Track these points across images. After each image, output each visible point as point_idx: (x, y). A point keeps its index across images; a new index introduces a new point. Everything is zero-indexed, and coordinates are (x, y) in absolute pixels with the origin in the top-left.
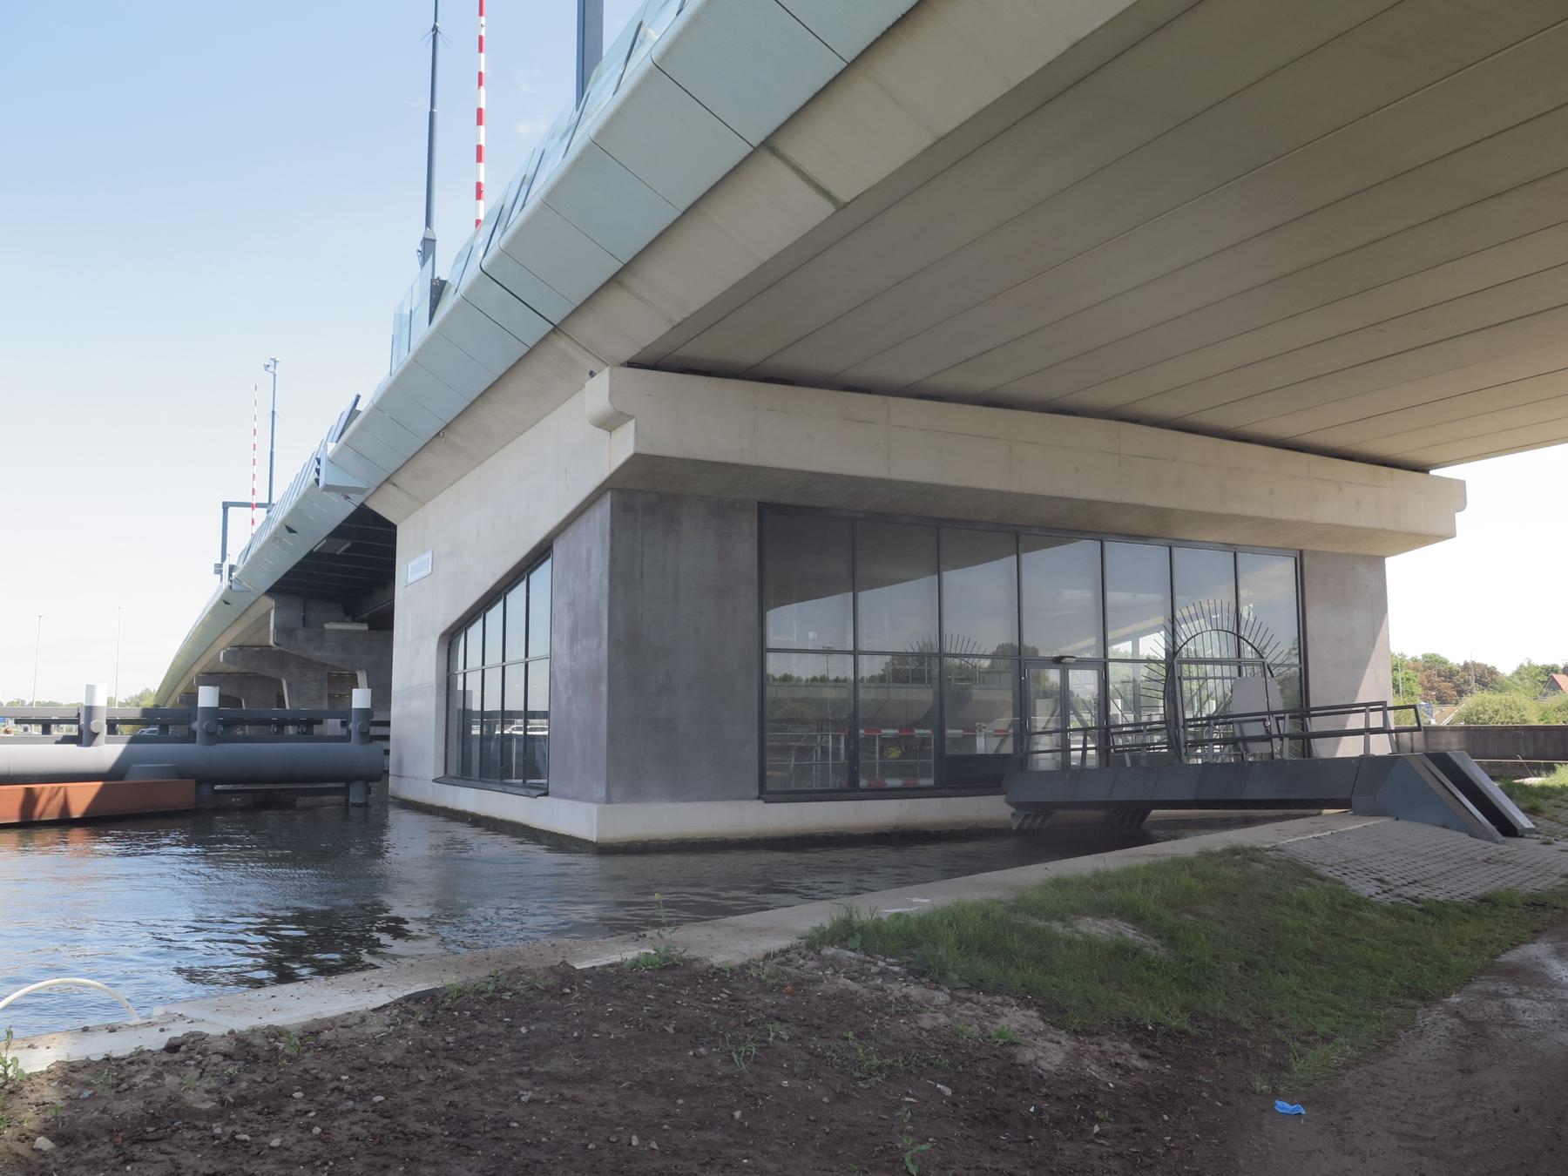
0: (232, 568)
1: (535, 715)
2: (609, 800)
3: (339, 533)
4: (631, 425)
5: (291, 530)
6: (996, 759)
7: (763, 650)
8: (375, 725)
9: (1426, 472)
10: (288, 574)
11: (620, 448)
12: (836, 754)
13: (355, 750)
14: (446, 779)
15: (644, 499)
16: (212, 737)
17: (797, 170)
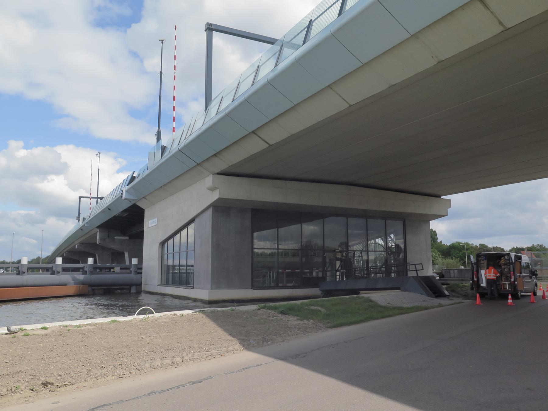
0: (84, 219)
1: (189, 266)
2: (211, 289)
3: (125, 211)
4: (218, 190)
5: (110, 210)
6: (318, 278)
7: (253, 248)
8: (139, 269)
9: (438, 196)
10: (105, 222)
11: (215, 196)
12: (273, 277)
13: (132, 277)
14: (162, 284)
15: (221, 208)
16: (92, 273)
17: (260, 137)
